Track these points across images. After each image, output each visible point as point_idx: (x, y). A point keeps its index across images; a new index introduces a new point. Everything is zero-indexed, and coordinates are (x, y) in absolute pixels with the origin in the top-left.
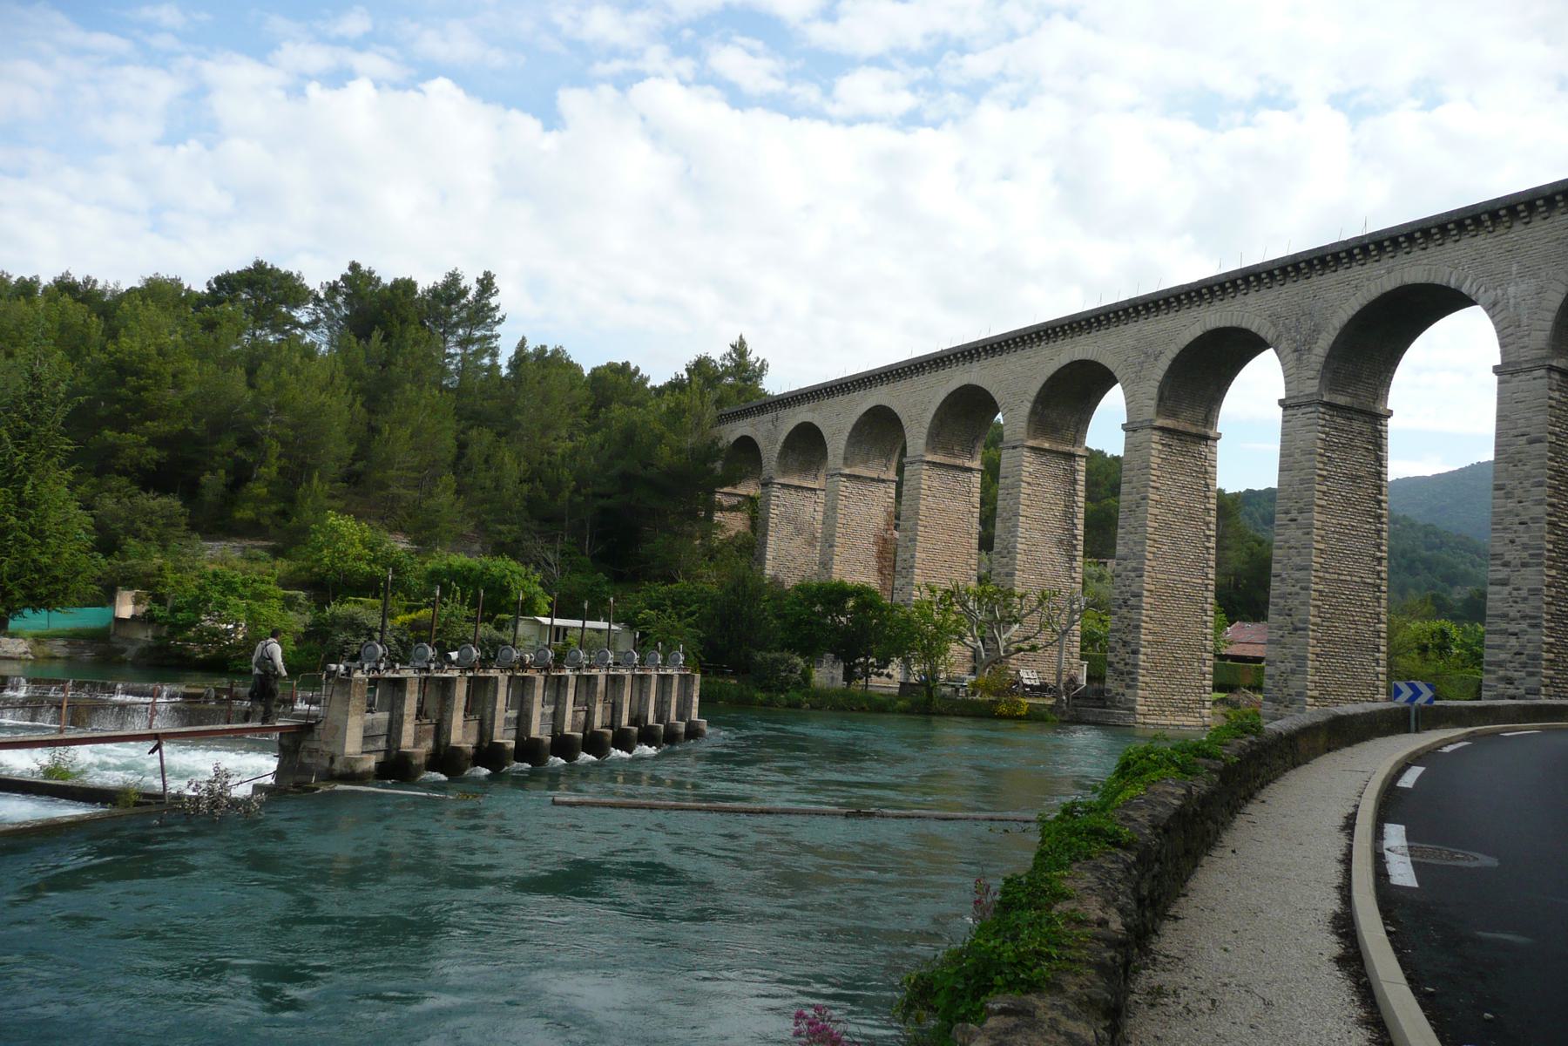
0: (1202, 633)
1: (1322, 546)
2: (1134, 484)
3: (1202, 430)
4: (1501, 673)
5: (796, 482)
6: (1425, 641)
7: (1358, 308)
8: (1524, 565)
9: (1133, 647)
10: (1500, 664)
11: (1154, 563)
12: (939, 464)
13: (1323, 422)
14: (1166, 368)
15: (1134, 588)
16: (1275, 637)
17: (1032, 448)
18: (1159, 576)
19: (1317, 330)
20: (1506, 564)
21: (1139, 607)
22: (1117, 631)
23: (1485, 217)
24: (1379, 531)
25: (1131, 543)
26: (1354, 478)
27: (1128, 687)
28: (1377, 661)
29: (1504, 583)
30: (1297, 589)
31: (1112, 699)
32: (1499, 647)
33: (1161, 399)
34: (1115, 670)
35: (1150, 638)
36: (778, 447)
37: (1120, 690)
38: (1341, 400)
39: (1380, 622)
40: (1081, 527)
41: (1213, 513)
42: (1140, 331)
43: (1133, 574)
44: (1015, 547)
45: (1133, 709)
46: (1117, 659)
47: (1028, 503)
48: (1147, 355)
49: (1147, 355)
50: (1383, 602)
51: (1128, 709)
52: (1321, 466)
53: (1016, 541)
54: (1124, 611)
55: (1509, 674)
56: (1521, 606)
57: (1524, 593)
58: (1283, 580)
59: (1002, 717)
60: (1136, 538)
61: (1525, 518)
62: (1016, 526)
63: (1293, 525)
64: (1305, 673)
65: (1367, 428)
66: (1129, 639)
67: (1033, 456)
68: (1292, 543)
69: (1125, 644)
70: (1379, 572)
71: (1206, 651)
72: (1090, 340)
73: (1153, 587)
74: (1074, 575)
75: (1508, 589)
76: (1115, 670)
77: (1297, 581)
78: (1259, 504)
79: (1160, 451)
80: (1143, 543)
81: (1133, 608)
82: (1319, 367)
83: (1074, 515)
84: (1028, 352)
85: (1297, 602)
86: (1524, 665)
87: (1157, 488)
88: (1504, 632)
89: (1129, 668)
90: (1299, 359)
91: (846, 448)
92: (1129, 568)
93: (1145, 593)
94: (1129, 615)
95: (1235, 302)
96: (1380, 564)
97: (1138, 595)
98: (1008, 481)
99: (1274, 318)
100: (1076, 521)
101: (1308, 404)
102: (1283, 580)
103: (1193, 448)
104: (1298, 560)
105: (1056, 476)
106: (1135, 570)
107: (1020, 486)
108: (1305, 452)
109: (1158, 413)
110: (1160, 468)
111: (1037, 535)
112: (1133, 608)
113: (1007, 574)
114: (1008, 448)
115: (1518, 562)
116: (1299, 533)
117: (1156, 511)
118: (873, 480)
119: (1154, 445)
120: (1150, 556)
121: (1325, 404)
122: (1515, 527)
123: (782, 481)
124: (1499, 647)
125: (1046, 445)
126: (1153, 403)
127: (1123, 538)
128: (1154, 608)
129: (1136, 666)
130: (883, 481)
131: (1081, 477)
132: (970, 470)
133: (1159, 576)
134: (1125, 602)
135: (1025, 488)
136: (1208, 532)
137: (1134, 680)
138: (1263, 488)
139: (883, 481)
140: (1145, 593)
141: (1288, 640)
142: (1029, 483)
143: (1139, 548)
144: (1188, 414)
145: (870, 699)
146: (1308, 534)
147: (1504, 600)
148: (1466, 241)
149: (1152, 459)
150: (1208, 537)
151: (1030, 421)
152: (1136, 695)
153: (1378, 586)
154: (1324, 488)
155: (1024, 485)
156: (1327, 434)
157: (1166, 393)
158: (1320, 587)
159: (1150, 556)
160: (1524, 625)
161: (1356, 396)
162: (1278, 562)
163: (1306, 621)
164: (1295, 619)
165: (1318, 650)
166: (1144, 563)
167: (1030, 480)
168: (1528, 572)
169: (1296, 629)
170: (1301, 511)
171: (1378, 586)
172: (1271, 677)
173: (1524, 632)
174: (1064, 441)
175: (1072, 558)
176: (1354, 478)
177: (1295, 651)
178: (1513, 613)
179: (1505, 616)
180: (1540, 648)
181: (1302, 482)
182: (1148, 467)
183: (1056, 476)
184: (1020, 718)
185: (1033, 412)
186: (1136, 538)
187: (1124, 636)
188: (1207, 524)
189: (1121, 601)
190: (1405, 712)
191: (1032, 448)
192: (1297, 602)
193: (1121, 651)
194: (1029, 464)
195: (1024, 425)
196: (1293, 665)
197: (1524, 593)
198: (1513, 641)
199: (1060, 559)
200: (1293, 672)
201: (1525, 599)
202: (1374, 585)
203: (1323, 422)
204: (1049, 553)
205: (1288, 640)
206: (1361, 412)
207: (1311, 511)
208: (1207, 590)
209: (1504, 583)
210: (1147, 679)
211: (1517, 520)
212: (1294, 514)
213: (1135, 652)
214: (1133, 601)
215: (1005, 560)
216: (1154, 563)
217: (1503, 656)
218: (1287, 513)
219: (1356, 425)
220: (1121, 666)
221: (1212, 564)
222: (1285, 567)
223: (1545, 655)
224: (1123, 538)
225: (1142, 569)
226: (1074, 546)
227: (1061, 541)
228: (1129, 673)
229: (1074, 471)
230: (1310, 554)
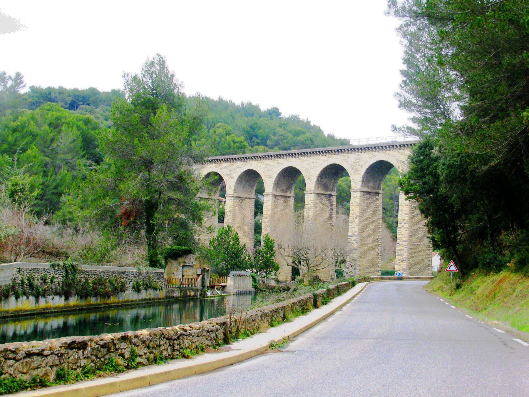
2: (354, 211)
3: (377, 191)
12: (279, 195)
22: (349, 261)
25: (353, 232)
30: (404, 248)
41: (381, 220)
43: (354, 242)
46: (349, 271)
63: (403, 228)
66: (353, 264)
68: (402, 233)
72: (338, 157)
77: (404, 245)
85: (404, 252)
89: (353, 274)
91: (235, 185)
92: (353, 239)
95: (386, 153)
102: (400, 245)
103: (374, 198)
114: (308, 193)
118: (246, 198)
126: (360, 183)
130: (250, 198)
132: (290, 197)
133: (363, 242)
139: (250, 198)
145: (61, 315)
151: (316, 183)
157: (365, 179)
168: (243, 314)
174: (330, 190)
185: (318, 180)
187: (351, 263)
192: (404, 252)
212: (403, 224)
218: (401, 224)
220: (351, 274)
224: (351, 230)
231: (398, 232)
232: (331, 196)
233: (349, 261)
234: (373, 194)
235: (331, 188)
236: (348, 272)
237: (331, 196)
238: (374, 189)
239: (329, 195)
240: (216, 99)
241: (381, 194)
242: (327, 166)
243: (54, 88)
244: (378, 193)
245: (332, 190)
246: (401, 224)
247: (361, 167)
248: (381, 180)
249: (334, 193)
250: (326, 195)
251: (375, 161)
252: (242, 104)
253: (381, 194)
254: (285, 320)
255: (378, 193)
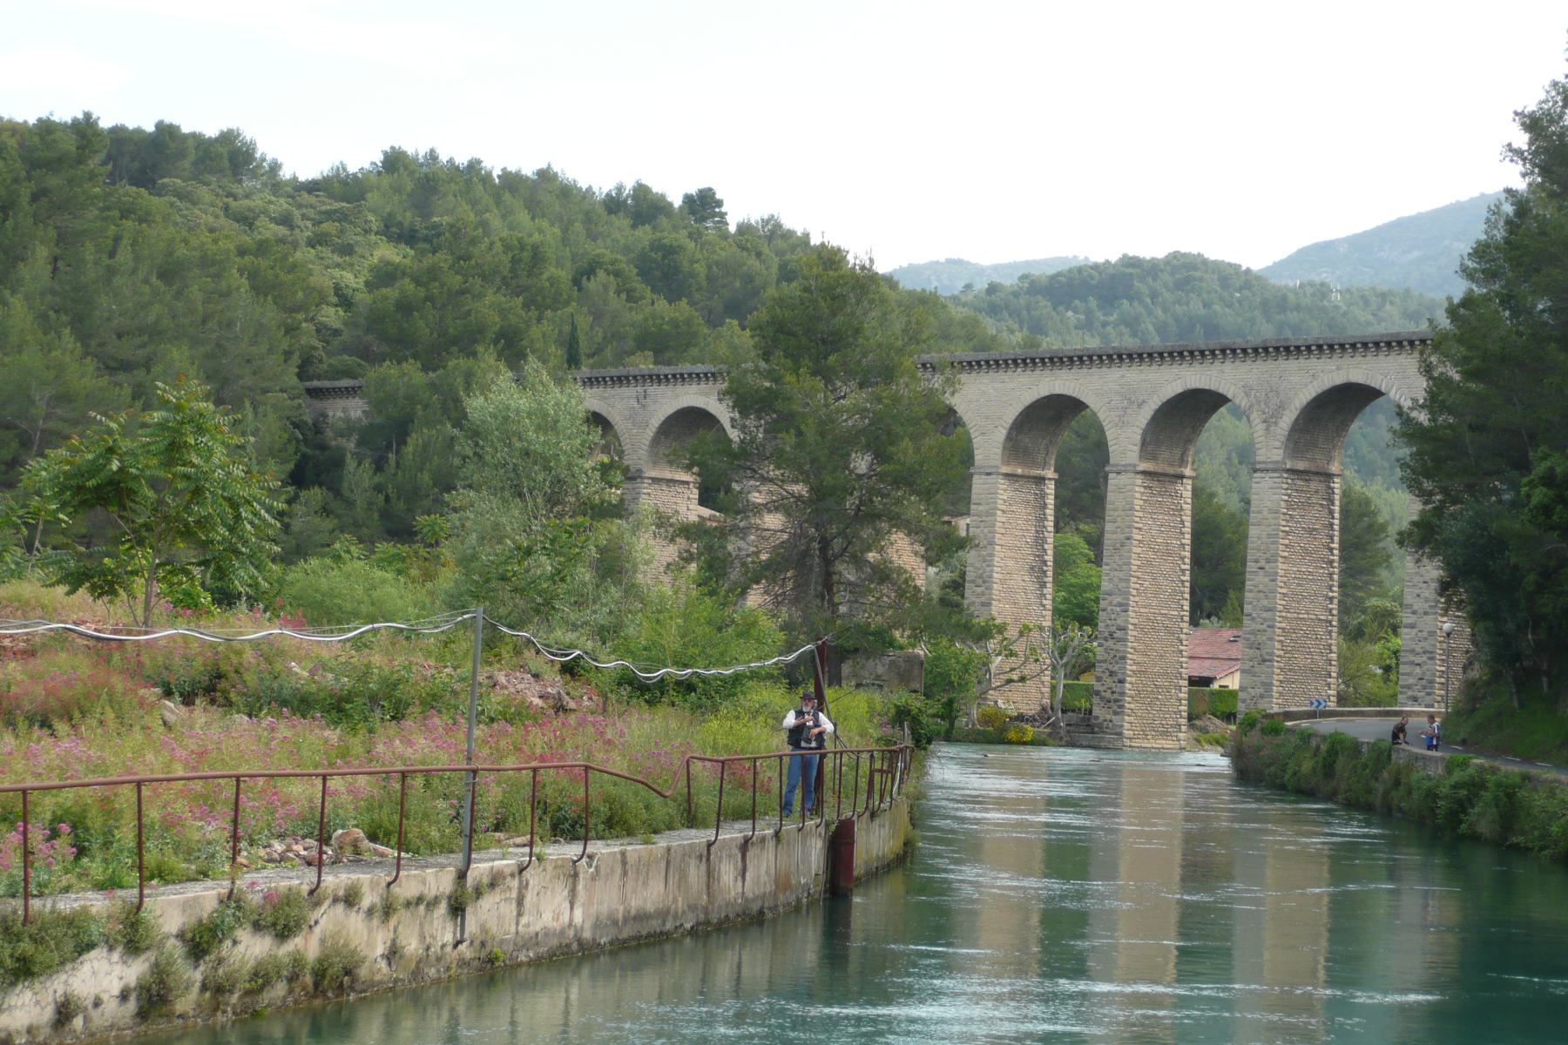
0: (1178, 662)
1: (1284, 591)
3: (1178, 470)
4: (1410, 693)
5: (668, 475)
6: (1388, 662)
7: (1314, 395)
8: (1426, 613)
9: (1120, 676)
10: (1409, 687)
11: (1137, 599)
13: (1285, 486)
14: (1149, 417)
15: (1120, 622)
16: (1247, 667)
17: (1007, 475)
18: (1142, 610)
19: (1282, 407)
20: (1414, 613)
21: (1125, 640)
22: (1105, 661)
23: (1405, 343)
24: (1331, 575)
25: (1116, 580)
26: (1311, 531)
27: (1116, 713)
28: (1329, 685)
29: (1412, 626)
30: (1264, 627)
31: (1100, 726)
32: (1408, 674)
33: (1144, 443)
34: (1102, 698)
35: (1134, 668)
36: (650, 433)
37: (1108, 717)
38: (1301, 465)
39: (1331, 652)
40: (1050, 552)
42: (1123, 376)
43: (1118, 609)
44: (991, 577)
45: (1120, 734)
47: (1003, 531)
48: (1131, 403)
49: (1131, 403)
50: (1334, 635)
51: (1116, 734)
52: (1284, 523)
53: (992, 571)
54: (1110, 643)
55: (1415, 694)
56: (1423, 644)
57: (1425, 634)
58: (1253, 619)
59: (1010, 742)
60: (1121, 575)
61: (1427, 579)
62: (992, 555)
63: (1260, 571)
64: (1272, 696)
65: (1321, 487)
66: (1116, 668)
67: (1007, 482)
68: (1261, 587)
69: (1112, 674)
70: (1331, 610)
71: (1182, 678)
73: (1136, 621)
74: (1045, 602)
75: (1415, 631)
76: (1102, 698)
77: (1265, 620)
78: (1154, 295)
79: (1142, 494)
80: (1128, 581)
81: (1119, 640)
82: (1283, 439)
83: (1044, 540)
84: (1001, 375)
86: (1424, 687)
87: (1140, 529)
88: (1412, 663)
89: (1115, 696)
90: (1267, 429)
92: (1115, 602)
93: (1131, 627)
94: (1115, 647)
95: (1213, 367)
96: (1331, 603)
97: (1124, 629)
98: (981, 508)
99: (1247, 389)
100: (1046, 546)
101: (1274, 470)
102: (1253, 619)
103: (1170, 487)
104: (1265, 602)
105: (1028, 502)
106: (1120, 605)
107: (995, 514)
108: (1272, 511)
109: (1141, 458)
110: (1142, 510)
111: (1011, 563)
112: (1119, 640)
113: (983, 604)
114: (981, 474)
115: (1421, 611)
116: (1266, 579)
117: (1139, 550)
119: (1137, 489)
120: (1134, 592)
121: (1288, 471)
122: (1421, 585)
123: (654, 474)
124: (1408, 674)
125: (1019, 471)
126: (1137, 448)
127: (1108, 575)
128: (1137, 639)
129: (1123, 694)
131: (1050, 501)
133: (1142, 610)
134: (1111, 634)
135: (1000, 517)
136: (1183, 567)
137: (1121, 707)
138: (1160, 252)
140: (1131, 627)
141: (1257, 669)
142: (1003, 511)
143: (1124, 585)
144: (1165, 455)
146: (1273, 580)
147: (1412, 639)
148: (1393, 357)
149: (1136, 502)
150: (1183, 571)
152: (1123, 720)
153: (1330, 622)
154: (1287, 542)
155: (999, 513)
156: (1289, 496)
158: (1283, 625)
159: (1134, 592)
160: (1425, 658)
161: (1313, 460)
162: (1250, 603)
163: (1272, 654)
164: (1264, 652)
165: (1281, 677)
166: (1128, 599)
167: (1004, 507)
169: (1264, 661)
170: (1268, 561)
171: (1330, 622)
172: (1244, 701)
173: (1425, 663)
174: (1035, 464)
175: (1043, 585)
176: (1311, 531)
177: (1263, 678)
178: (1418, 649)
179: (1412, 651)
180: (1434, 675)
181: (1269, 536)
182: (1132, 509)
183: (1028, 502)
184: (1025, 743)
185: (1009, 438)
186: (1121, 575)
187: (1110, 667)
188: (1182, 558)
189: (1107, 634)
190: (1315, 712)
191: (1007, 475)
193: (1109, 681)
194: (1004, 492)
195: (999, 451)
196: (1262, 691)
197: (1425, 634)
198: (1418, 670)
199: (1032, 587)
200: (1262, 696)
201: (1425, 639)
202: (1326, 621)
203: (1285, 486)
204: (1022, 581)
205: (1257, 669)
206: (1317, 473)
207: (1276, 561)
208: (1183, 621)
209: (1412, 626)
210: (1132, 706)
211: (1422, 580)
212: (1262, 563)
213: (1122, 681)
214: (1118, 634)
215: (979, 590)
216: (1137, 599)
217: (1411, 681)
218: (1257, 561)
219: (1314, 485)
220: (1108, 695)
221: (1187, 596)
222: (1254, 608)
223: (1438, 680)
224: (1108, 575)
225: (1127, 605)
226: (1045, 572)
227: (1032, 568)
228: (1116, 701)
229: (1043, 496)
230: (1275, 598)
231: (1248, 583)
232: (1041, 480)
233: (1105, 661)
234: (1167, 479)
235: (1040, 459)
236: (1101, 689)
237: (1041, 480)
238: (1171, 464)
239: (1035, 478)
240: (150, 128)
241: (1189, 478)
242: (1038, 401)
243: (1107, 262)
244: (1182, 477)
245: (1044, 466)
246: (1257, 561)
247: (1139, 406)
248: (1189, 441)
249: (1050, 473)
250: (1029, 477)
251: (1180, 390)
252: (589, 189)
253: (1189, 478)
254: (189, 935)
255: (1182, 477)
